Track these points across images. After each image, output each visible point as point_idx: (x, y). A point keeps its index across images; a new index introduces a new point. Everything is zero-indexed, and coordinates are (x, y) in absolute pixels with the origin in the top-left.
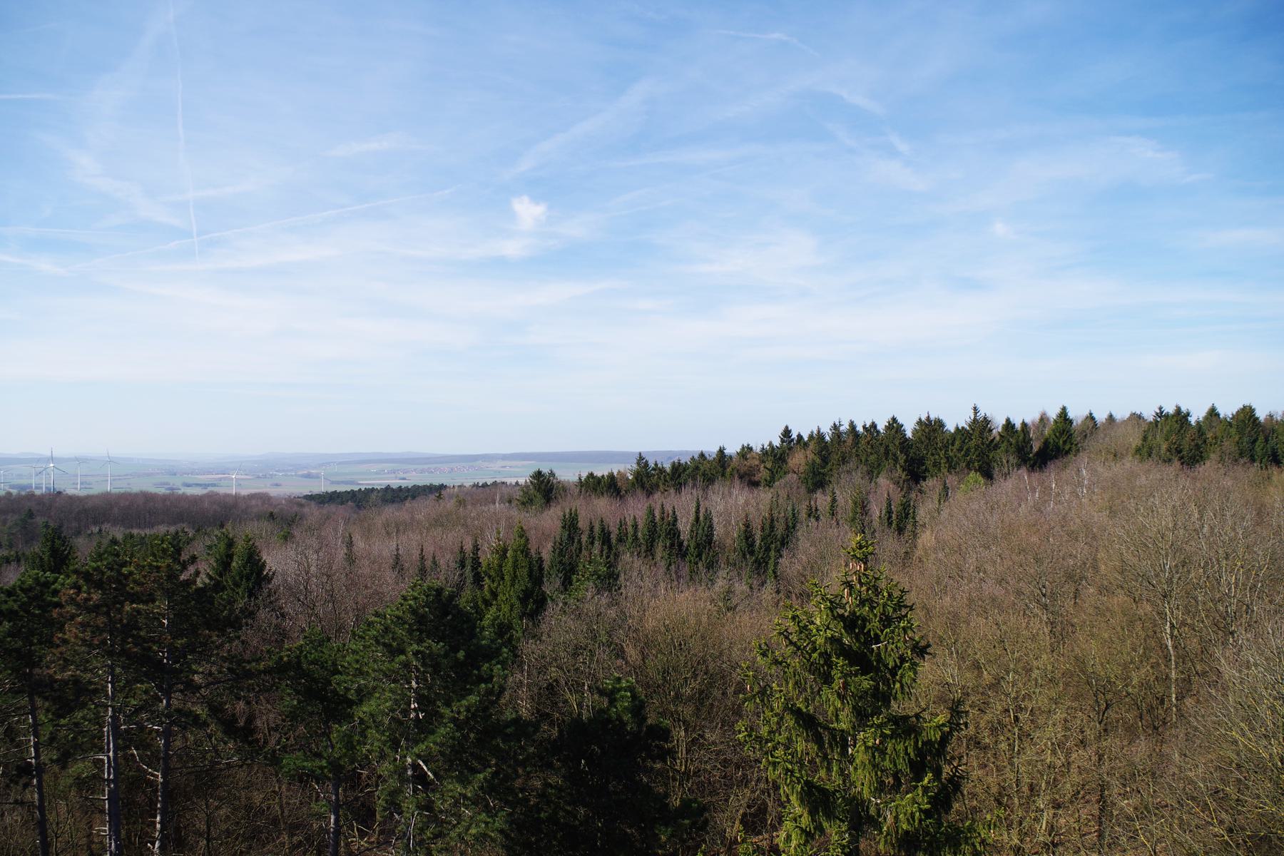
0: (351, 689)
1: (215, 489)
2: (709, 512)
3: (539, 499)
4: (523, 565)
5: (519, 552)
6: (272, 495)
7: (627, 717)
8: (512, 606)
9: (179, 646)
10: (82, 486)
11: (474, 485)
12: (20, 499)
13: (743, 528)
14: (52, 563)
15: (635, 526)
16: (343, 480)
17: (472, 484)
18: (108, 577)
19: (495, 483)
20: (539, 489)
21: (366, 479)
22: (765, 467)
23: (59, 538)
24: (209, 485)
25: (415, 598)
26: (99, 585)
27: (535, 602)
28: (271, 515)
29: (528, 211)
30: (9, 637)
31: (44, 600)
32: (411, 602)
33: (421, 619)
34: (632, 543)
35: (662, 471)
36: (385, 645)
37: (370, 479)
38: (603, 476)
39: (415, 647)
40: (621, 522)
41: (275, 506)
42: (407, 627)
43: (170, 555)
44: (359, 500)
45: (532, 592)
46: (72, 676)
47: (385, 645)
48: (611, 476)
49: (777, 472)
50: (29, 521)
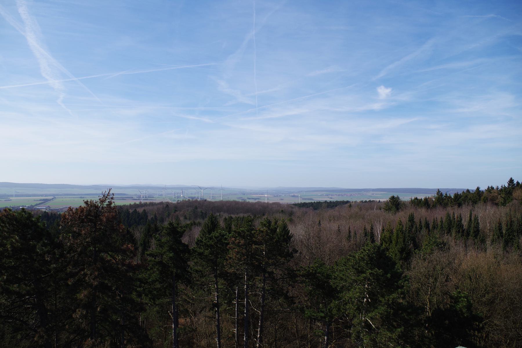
0: (339, 286)
2: (477, 217)
7: (464, 310)
8: (396, 254)
9: (270, 263)
10: (213, 198)
13: (498, 225)
14: (211, 227)
15: (442, 222)
16: (307, 198)
19: (370, 201)
20: (393, 204)
21: (316, 198)
22: (501, 197)
25: (369, 250)
26: (243, 237)
28: (282, 211)
29: (383, 92)
30: (210, 255)
32: (367, 251)
33: (371, 259)
34: (440, 229)
35: (450, 197)
36: (356, 269)
37: (318, 198)
38: (421, 199)
39: (370, 271)
40: (434, 219)
42: (366, 262)
44: (316, 206)
46: (233, 271)
47: (356, 269)
48: (426, 199)
49: (507, 199)
50: (196, 210)
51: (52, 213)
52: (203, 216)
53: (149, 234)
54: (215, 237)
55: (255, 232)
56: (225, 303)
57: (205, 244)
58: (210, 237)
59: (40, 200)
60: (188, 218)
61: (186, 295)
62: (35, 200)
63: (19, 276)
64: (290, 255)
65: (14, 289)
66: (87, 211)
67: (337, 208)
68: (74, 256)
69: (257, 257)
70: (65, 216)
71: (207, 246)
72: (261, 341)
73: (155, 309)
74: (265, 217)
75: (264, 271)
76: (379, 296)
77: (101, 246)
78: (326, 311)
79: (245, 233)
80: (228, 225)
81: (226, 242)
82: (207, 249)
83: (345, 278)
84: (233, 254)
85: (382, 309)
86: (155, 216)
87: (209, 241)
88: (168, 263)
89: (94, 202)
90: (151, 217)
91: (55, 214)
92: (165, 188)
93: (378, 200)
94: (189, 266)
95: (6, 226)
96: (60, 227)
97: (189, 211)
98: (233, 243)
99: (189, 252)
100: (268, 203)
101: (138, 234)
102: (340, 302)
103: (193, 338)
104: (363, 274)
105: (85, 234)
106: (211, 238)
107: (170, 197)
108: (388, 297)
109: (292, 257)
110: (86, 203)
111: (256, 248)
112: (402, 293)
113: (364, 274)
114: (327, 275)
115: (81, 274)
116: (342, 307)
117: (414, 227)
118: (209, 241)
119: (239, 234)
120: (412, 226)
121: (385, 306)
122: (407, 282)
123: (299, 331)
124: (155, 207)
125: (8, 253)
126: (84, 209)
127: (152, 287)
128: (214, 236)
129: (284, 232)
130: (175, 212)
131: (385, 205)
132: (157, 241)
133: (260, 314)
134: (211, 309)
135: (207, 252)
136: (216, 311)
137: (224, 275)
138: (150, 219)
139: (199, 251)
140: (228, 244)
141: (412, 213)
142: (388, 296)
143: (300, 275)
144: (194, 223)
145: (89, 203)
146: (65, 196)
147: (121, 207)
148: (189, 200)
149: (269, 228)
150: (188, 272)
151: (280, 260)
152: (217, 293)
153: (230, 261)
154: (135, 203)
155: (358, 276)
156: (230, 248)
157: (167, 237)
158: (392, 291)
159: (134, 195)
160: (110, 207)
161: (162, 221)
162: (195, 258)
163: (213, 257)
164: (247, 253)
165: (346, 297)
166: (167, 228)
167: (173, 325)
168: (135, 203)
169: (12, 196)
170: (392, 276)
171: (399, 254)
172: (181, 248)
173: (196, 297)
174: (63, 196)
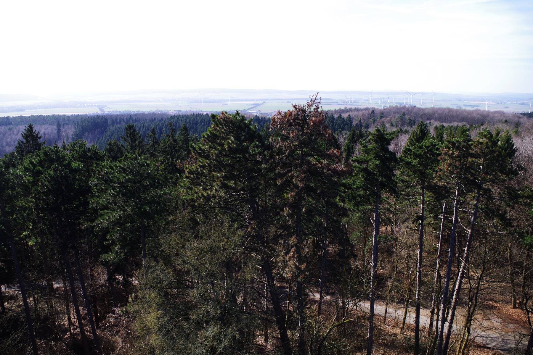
12: (401, 108)
26: (458, 148)
31: (433, 152)
41: (507, 117)
51: (262, 117)
52: (411, 123)
54: (426, 147)
55: (473, 143)
56: (430, 217)
59: (252, 105)
60: (394, 124)
61: (389, 204)
62: (247, 105)
63: (235, 173)
65: (231, 185)
66: (295, 115)
68: (282, 158)
69: (472, 171)
70: (274, 119)
71: (416, 156)
72: (467, 261)
73: (357, 215)
74: (484, 127)
75: (480, 187)
77: (308, 149)
79: (460, 143)
81: (437, 152)
82: (415, 159)
86: (360, 122)
87: (418, 151)
90: (356, 122)
91: (265, 118)
94: (395, 175)
95: (223, 128)
96: (270, 130)
97: (397, 117)
98: (446, 154)
99: (396, 160)
100: (488, 112)
101: (343, 140)
103: (393, 247)
105: (293, 137)
106: (420, 148)
109: (517, 174)
110: (295, 107)
111: (472, 161)
119: (453, 144)
125: (226, 153)
129: (506, 145)
130: (381, 119)
132: (363, 147)
134: (414, 221)
135: (415, 162)
136: (420, 224)
138: (355, 125)
140: (440, 154)
144: (401, 130)
145: (297, 107)
147: (327, 113)
148: (397, 106)
149: (490, 140)
150: (394, 181)
151: (500, 176)
152: (423, 205)
153: (440, 173)
156: (441, 159)
160: (317, 112)
161: (367, 127)
163: (421, 168)
164: (461, 166)
169: (228, 101)
173: (400, 207)
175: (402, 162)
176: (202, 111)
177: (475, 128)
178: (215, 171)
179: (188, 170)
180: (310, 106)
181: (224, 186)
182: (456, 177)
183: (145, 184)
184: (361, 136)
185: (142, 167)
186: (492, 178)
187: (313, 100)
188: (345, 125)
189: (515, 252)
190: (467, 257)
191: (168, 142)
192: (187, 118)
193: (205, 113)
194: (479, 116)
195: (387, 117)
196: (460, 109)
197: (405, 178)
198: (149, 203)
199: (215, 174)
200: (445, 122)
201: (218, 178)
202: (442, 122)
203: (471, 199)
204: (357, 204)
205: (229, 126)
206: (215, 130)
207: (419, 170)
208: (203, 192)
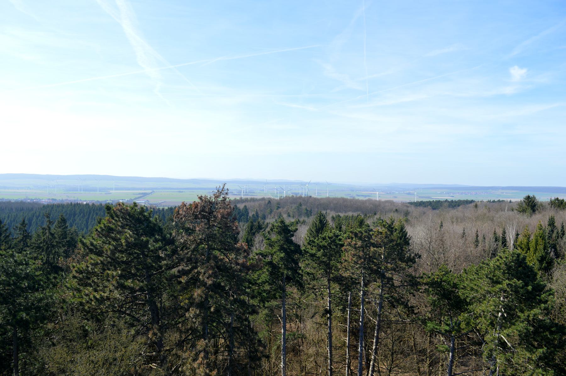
1: (371, 198)
3: (529, 210)
4: (541, 243)
5: (539, 237)
6: (395, 201)
11: (488, 201)
17: (487, 200)
18: (365, 235)
19: (499, 201)
21: (435, 196)
23: (322, 216)
24: (367, 196)
25: (506, 258)
26: (360, 239)
27: (547, 263)
28: (396, 210)
29: (517, 73)
31: (336, 243)
33: (509, 268)
36: (490, 278)
37: (437, 196)
39: (507, 281)
41: (397, 206)
43: (387, 228)
44: (435, 205)
45: (546, 258)
46: (349, 276)
47: (490, 278)
53: (252, 232)
54: (329, 237)
55: (374, 233)
57: (318, 244)
58: (323, 237)
59: (139, 194)
60: (291, 215)
62: (134, 194)
64: (411, 260)
65: (129, 284)
67: (460, 208)
68: (187, 253)
71: (320, 247)
72: (376, 353)
73: (264, 312)
74: (377, 216)
75: (383, 276)
76: (517, 310)
78: (452, 324)
80: (339, 224)
81: (340, 243)
83: (476, 289)
84: (349, 257)
85: (521, 326)
86: (257, 213)
87: (321, 242)
88: (278, 264)
89: (208, 198)
90: (253, 213)
92: (266, 183)
93: (509, 200)
95: (120, 221)
97: (293, 208)
98: (350, 244)
99: (300, 252)
100: (380, 201)
102: (470, 315)
104: (499, 285)
105: (199, 231)
106: (324, 239)
107: (271, 193)
108: (529, 312)
110: (200, 198)
112: (546, 309)
113: (500, 284)
114: (454, 283)
115: (194, 272)
116: (472, 320)
117: (555, 231)
118: (321, 242)
119: (356, 235)
120: (553, 231)
121: (525, 322)
122: (552, 296)
123: (417, 344)
124: (256, 203)
126: (198, 205)
127: (261, 288)
128: (328, 236)
129: (401, 234)
131: (518, 206)
132: (267, 240)
133: (376, 324)
135: (319, 254)
137: (339, 280)
138: (251, 216)
139: (310, 252)
140: (342, 245)
141: (553, 216)
142: (528, 311)
143: (423, 283)
146: (163, 190)
150: (299, 274)
152: (330, 298)
154: (235, 199)
155: (493, 286)
157: (278, 236)
158: (534, 306)
159: (234, 190)
162: (306, 259)
163: (325, 259)
165: (478, 310)
166: (278, 226)
167: (375, 339)
168: (235, 199)
169: (112, 189)
170: (533, 289)
171: (539, 264)
172: (292, 248)
173: (306, 301)
174: (161, 190)
175: (306, 254)
176: (81, 200)
177: (369, 217)
178: (109, 269)
179: (76, 269)
180: (217, 197)
181: (121, 287)
182: (360, 268)
183: (23, 286)
184: (260, 228)
185: (19, 266)
186: (393, 267)
187: (220, 191)
188: (241, 216)
189: (419, 340)
190: (376, 349)
191: (43, 236)
192: (63, 208)
193: (85, 203)
194: (371, 205)
195: (283, 208)
196: (354, 199)
197: (308, 270)
198: (27, 309)
199: (109, 272)
200: (340, 212)
201: (113, 277)
202: (338, 213)
203: (375, 289)
204: (263, 300)
205: (126, 219)
206: (110, 222)
207: (324, 262)
208: (94, 293)
